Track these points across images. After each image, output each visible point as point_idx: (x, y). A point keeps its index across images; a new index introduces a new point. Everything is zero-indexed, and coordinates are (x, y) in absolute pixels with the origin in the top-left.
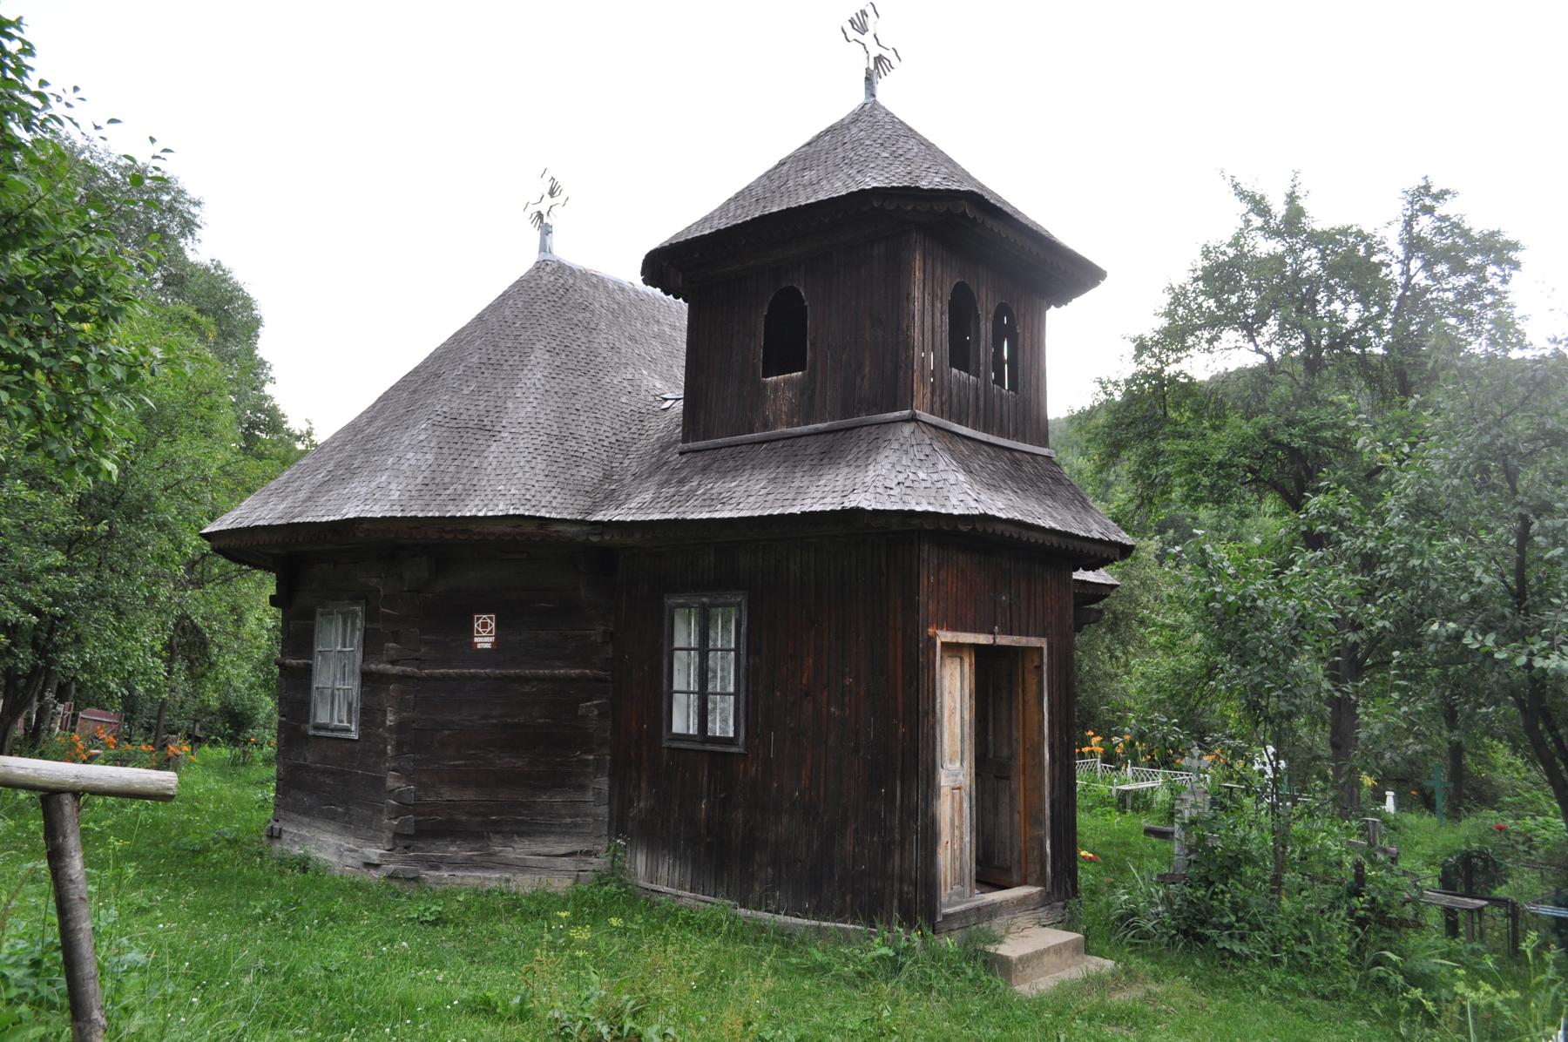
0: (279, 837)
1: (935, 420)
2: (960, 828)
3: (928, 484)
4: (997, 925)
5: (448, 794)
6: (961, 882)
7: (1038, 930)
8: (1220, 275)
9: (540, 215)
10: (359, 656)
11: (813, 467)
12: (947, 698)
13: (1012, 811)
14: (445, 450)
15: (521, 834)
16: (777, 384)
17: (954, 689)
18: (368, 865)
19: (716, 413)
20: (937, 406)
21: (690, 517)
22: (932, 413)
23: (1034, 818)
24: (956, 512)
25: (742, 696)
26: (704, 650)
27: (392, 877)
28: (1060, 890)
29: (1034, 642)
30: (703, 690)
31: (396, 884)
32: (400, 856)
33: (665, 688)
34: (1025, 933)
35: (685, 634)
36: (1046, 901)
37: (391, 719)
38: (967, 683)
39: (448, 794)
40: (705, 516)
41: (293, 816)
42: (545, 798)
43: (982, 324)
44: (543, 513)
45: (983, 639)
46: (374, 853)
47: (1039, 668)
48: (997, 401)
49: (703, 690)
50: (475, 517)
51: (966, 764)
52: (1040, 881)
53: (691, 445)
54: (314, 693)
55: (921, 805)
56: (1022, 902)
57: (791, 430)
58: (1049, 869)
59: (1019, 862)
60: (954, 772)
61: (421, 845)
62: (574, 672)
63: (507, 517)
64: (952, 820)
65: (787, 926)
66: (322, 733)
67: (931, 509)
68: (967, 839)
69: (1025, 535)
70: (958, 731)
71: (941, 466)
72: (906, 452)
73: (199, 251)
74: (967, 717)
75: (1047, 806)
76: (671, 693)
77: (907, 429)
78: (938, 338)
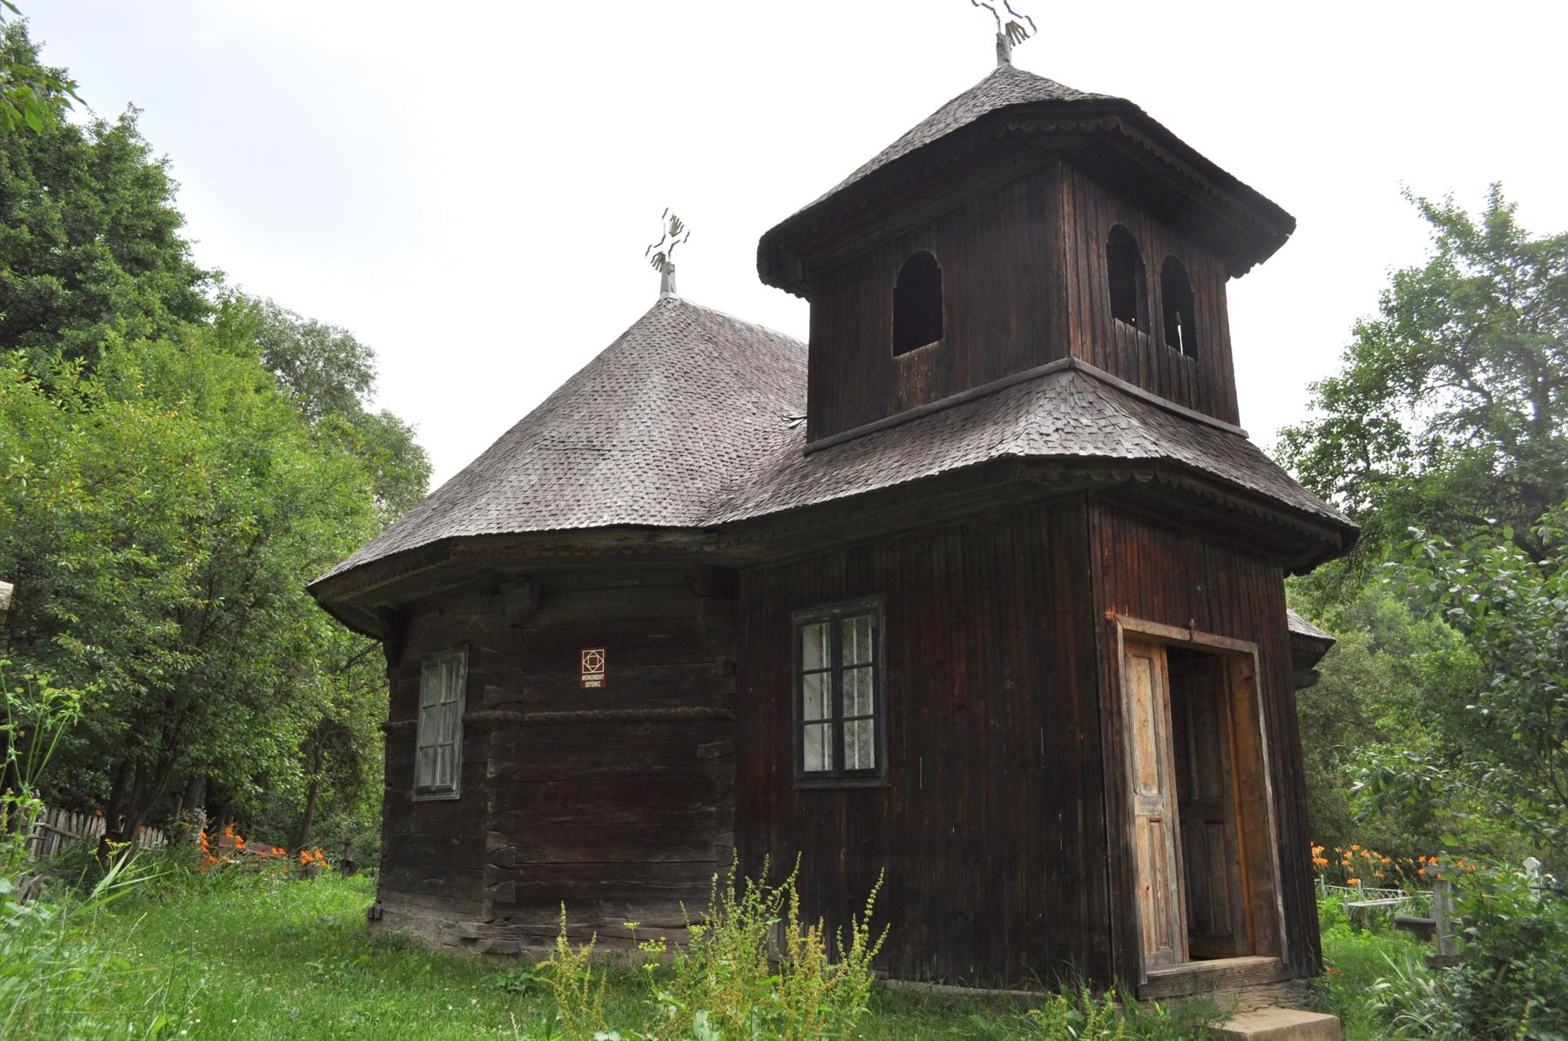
0: (380, 919)
1: (1098, 372)
2: (1164, 872)
3: (1094, 430)
4: (1221, 998)
5: (553, 856)
6: (1169, 941)
7: (1274, 1010)
8: (1416, 300)
9: (661, 257)
10: (461, 706)
11: (953, 433)
12: (1135, 707)
13: (1229, 862)
14: (551, 471)
15: (636, 902)
16: (910, 362)
17: (1143, 697)
18: (468, 941)
19: (845, 390)
20: (1100, 357)
21: (811, 502)
22: (1094, 363)
23: (1259, 869)
24: (1130, 456)
25: (883, 718)
26: (837, 669)
27: (490, 952)
28: (1300, 964)
29: (1241, 645)
30: (837, 725)
31: (494, 961)
32: (500, 930)
33: (794, 718)
34: (1260, 1012)
35: (815, 654)
36: (1283, 976)
37: (491, 772)
38: (1159, 680)
39: (553, 856)
40: (829, 498)
41: (396, 894)
42: (660, 858)
43: (1148, 274)
44: (651, 522)
45: (1176, 633)
46: (471, 927)
47: (1250, 679)
48: (1174, 368)
49: (837, 725)
50: (576, 530)
51: (1166, 791)
52: (1274, 949)
53: (817, 443)
54: (419, 755)
55: (1110, 831)
56: (1252, 972)
57: (928, 406)
58: (1283, 934)
59: (1244, 927)
60: (1151, 801)
61: (522, 915)
62: (692, 711)
63: (611, 527)
64: (1153, 861)
65: (948, 996)
66: (426, 798)
67: (1098, 453)
68: (1173, 887)
69: (1221, 496)
70: (1153, 749)
71: (1109, 411)
72: (1065, 401)
73: (372, 404)
74: (1162, 733)
75: (1275, 851)
76: (802, 724)
77: (1065, 379)
78: (1095, 282)
